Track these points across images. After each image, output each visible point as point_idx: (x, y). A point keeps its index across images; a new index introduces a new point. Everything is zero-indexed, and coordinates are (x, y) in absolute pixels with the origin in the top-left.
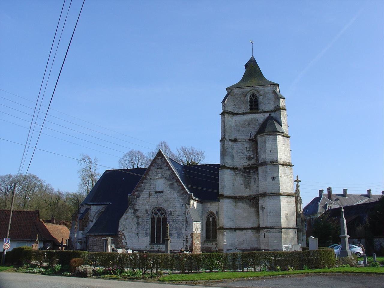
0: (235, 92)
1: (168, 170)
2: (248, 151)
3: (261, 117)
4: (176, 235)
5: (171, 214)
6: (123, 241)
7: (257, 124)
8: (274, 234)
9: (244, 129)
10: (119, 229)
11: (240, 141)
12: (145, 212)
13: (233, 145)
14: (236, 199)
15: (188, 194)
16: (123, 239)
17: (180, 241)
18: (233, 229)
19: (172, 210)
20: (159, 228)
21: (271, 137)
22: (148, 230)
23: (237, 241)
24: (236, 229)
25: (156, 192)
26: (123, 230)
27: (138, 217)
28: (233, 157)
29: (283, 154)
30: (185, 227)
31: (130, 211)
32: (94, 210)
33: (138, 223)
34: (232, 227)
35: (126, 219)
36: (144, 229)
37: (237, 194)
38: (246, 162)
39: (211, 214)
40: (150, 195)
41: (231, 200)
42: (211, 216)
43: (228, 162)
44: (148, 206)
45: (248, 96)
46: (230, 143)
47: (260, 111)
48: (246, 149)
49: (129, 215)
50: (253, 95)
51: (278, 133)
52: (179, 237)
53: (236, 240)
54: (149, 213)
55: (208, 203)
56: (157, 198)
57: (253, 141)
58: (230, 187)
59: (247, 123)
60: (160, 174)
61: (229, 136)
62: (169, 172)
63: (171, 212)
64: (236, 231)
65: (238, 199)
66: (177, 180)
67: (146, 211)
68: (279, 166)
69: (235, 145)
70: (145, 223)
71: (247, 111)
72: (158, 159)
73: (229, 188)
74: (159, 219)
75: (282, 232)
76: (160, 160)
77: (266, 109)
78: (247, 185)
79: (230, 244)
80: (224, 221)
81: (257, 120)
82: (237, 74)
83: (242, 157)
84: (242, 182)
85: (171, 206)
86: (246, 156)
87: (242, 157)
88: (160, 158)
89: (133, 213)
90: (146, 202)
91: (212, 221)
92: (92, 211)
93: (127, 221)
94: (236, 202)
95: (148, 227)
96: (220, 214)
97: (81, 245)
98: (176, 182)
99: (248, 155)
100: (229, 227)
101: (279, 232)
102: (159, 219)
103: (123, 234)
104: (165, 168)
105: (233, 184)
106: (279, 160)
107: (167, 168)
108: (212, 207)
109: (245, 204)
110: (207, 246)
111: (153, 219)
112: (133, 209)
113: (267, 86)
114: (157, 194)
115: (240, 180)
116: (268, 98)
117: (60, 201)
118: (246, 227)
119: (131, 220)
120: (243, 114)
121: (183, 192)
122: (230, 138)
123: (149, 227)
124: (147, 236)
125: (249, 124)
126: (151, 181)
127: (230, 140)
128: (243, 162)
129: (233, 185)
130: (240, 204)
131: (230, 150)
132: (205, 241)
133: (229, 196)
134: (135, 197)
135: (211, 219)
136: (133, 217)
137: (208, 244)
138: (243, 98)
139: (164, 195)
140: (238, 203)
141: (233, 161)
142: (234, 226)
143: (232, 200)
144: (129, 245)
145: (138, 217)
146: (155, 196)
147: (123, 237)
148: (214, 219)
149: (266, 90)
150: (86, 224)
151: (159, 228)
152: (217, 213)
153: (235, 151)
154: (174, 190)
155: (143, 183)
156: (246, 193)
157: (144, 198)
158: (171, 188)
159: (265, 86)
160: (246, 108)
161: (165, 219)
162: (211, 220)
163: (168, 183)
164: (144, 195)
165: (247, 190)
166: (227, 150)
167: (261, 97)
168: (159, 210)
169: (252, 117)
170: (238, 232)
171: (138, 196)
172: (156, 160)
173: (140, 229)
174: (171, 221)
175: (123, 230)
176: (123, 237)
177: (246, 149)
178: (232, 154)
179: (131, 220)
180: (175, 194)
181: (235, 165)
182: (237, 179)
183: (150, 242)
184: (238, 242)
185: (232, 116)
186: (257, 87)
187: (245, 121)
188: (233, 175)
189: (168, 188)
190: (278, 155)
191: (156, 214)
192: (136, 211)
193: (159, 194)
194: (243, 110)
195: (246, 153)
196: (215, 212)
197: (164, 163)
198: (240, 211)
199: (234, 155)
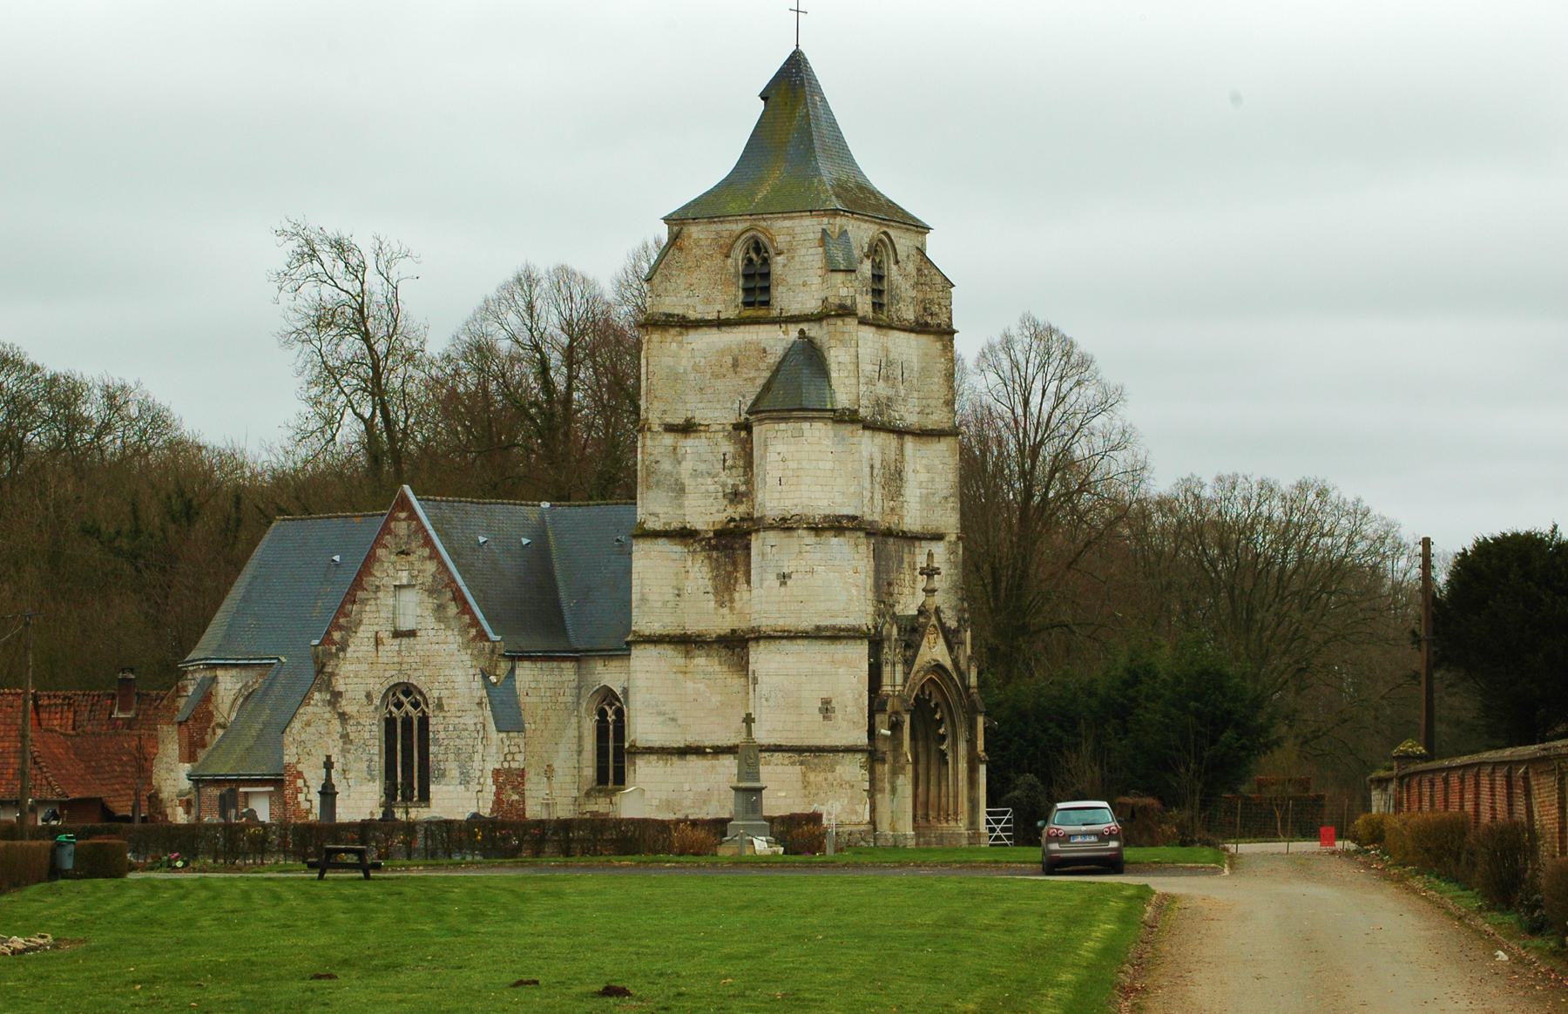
0: (695, 236)
1: (430, 558)
2: (732, 467)
3: (776, 339)
4: (456, 773)
5: (440, 706)
6: (301, 797)
7: (762, 366)
8: (780, 769)
9: (719, 384)
12: (364, 701)
14: (686, 642)
15: (488, 640)
16: (298, 790)
17: (468, 794)
19: (444, 693)
20: (408, 746)
21: (783, 426)
22: (376, 758)
25: (397, 634)
26: (298, 762)
27: (343, 717)
28: (680, 490)
30: (480, 747)
31: (317, 696)
32: (229, 686)
33: (345, 737)
34: (667, 744)
35: (308, 724)
36: (365, 757)
37: (693, 627)
39: (608, 695)
40: (378, 642)
42: (610, 705)
43: (658, 510)
44: (371, 681)
45: (738, 254)
46: (669, 439)
47: (775, 313)
49: (316, 710)
50: (758, 247)
52: (465, 779)
53: (687, 787)
54: (377, 702)
56: (399, 652)
57: (743, 428)
59: (729, 360)
60: (405, 574)
61: (665, 412)
62: (431, 567)
63: (440, 699)
66: (458, 597)
67: (369, 696)
69: (690, 444)
70: (367, 735)
71: (731, 313)
72: (398, 520)
74: (407, 721)
76: (404, 525)
77: (794, 309)
78: (725, 588)
80: (643, 728)
81: (765, 351)
82: (714, 155)
83: (712, 488)
84: (708, 584)
85: (442, 679)
86: (724, 485)
87: (712, 488)
88: (403, 515)
89: (329, 702)
90: (366, 667)
91: (615, 722)
92: (221, 687)
94: (687, 654)
95: (376, 750)
96: (631, 698)
97: (188, 812)
98: (454, 599)
99: (730, 482)
100: (657, 744)
102: (407, 721)
103: (300, 775)
104: (419, 552)
107: (427, 552)
108: (608, 675)
110: (595, 808)
111: (390, 723)
112: (327, 689)
114: (397, 641)
115: (698, 572)
116: (802, 263)
119: (323, 729)
120: (720, 324)
121: (473, 632)
122: (669, 420)
123: (376, 749)
124: (373, 779)
125: (735, 364)
126: (380, 594)
127: (670, 428)
128: (714, 510)
130: (701, 661)
131: (666, 466)
132: (588, 794)
134: (334, 649)
135: (610, 712)
136: (327, 716)
137: (600, 800)
138: (718, 259)
139: (419, 644)
141: (681, 506)
142: (679, 742)
145: (343, 717)
146: (391, 646)
147: (300, 783)
148: (620, 713)
149: (798, 230)
150: (203, 739)
151: (408, 746)
152: (625, 691)
153: (687, 466)
154: (448, 627)
155: (354, 602)
156: (719, 622)
157: (360, 654)
158: (439, 620)
160: (727, 301)
161: (424, 722)
162: (611, 718)
163: (430, 602)
164: (360, 644)
165: (725, 611)
167: (779, 258)
168: (407, 693)
169: (748, 337)
170: (694, 762)
171: (343, 647)
172: (392, 525)
173: (350, 757)
174: (441, 728)
175: (298, 762)
176: (300, 783)
179: (323, 729)
180: (451, 639)
181: (688, 519)
184: (691, 794)
185: (681, 334)
187: (722, 353)
188: (677, 556)
189: (430, 622)
191: (399, 705)
192: (337, 695)
193: (405, 641)
194: (719, 307)
195: (723, 476)
196: (618, 691)
197: (416, 532)
198: (701, 686)
199: (687, 482)
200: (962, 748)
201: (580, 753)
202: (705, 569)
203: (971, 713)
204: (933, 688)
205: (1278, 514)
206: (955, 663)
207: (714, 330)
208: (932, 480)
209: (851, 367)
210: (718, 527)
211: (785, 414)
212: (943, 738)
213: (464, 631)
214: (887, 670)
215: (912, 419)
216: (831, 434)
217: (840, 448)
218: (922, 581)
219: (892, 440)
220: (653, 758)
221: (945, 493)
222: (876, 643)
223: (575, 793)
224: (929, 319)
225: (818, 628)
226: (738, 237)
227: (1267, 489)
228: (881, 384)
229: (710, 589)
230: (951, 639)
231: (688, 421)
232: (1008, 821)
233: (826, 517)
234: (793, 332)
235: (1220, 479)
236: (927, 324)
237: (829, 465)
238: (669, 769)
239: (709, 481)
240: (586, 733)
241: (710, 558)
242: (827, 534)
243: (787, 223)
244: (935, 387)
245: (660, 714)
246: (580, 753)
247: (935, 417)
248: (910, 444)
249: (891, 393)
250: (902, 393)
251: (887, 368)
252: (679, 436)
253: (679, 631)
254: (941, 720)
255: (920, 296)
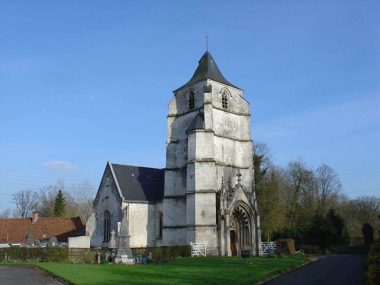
5: (112, 216)
10: (86, 230)
11: (181, 142)
13: (175, 146)
18: (173, 227)
23: (177, 238)
24: (176, 228)
29: (203, 151)
34: (171, 226)
38: (184, 161)
41: (171, 200)
48: (185, 149)
49: (92, 218)
51: (196, 130)
55: (158, 203)
58: (171, 188)
64: (177, 229)
65: (178, 198)
68: (196, 163)
73: (169, 188)
75: (195, 230)
79: (170, 241)
80: (166, 222)
87: (182, 157)
93: (91, 223)
94: (177, 202)
100: (169, 226)
101: (193, 230)
105: (175, 184)
106: (196, 157)
109: (183, 203)
113: (199, 82)
117: (327, 198)
118: (183, 225)
124: (101, 235)
129: (175, 186)
133: (170, 196)
140: (178, 202)
141: (175, 162)
142: (175, 225)
143: (173, 199)
144: (93, 243)
159: (198, 82)
166: (169, 152)
169: (190, 116)
170: (179, 230)
177: (185, 149)
178: (174, 156)
182: (178, 179)
183: (104, 240)
186: (194, 85)
188: (174, 175)
190: (196, 153)
199: (177, 156)
200: (254, 225)
201: (155, 228)
202: (181, 178)
203: (256, 215)
204: (241, 208)
205: (370, 201)
206: (250, 201)
207: (183, 116)
208: (245, 153)
209: (210, 118)
210: (183, 166)
211: (192, 131)
212: (247, 222)
213: (117, 196)
214: (221, 204)
215: (239, 137)
216: (204, 135)
217: (207, 139)
218: (237, 178)
219: (230, 142)
220: (167, 229)
221: (248, 156)
222: (218, 194)
223: (154, 239)
224: (243, 112)
225: (200, 190)
226: (187, 91)
227: (368, 198)
228: (226, 126)
229: (182, 183)
230: (247, 194)
231: (178, 140)
232: (193, 253)
233: (203, 159)
234: (198, 112)
235: (362, 196)
236: (242, 113)
237: (204, 144)
238: (172, 233)
239: (182, 155)
240: (157, 223)
241: (181, 175)
242: (203, 163)
243: (197, 85)
244: (245, 129)
245: (170, 217)
246: (155, 228)
247: (245, 137)
248: (237, 143)
249: (230, 129)
250: (235, 130)
251: (229, 123)
252: (175, 144)
253: (175, 195)
254: (246, 218)
255: (240, 106)
